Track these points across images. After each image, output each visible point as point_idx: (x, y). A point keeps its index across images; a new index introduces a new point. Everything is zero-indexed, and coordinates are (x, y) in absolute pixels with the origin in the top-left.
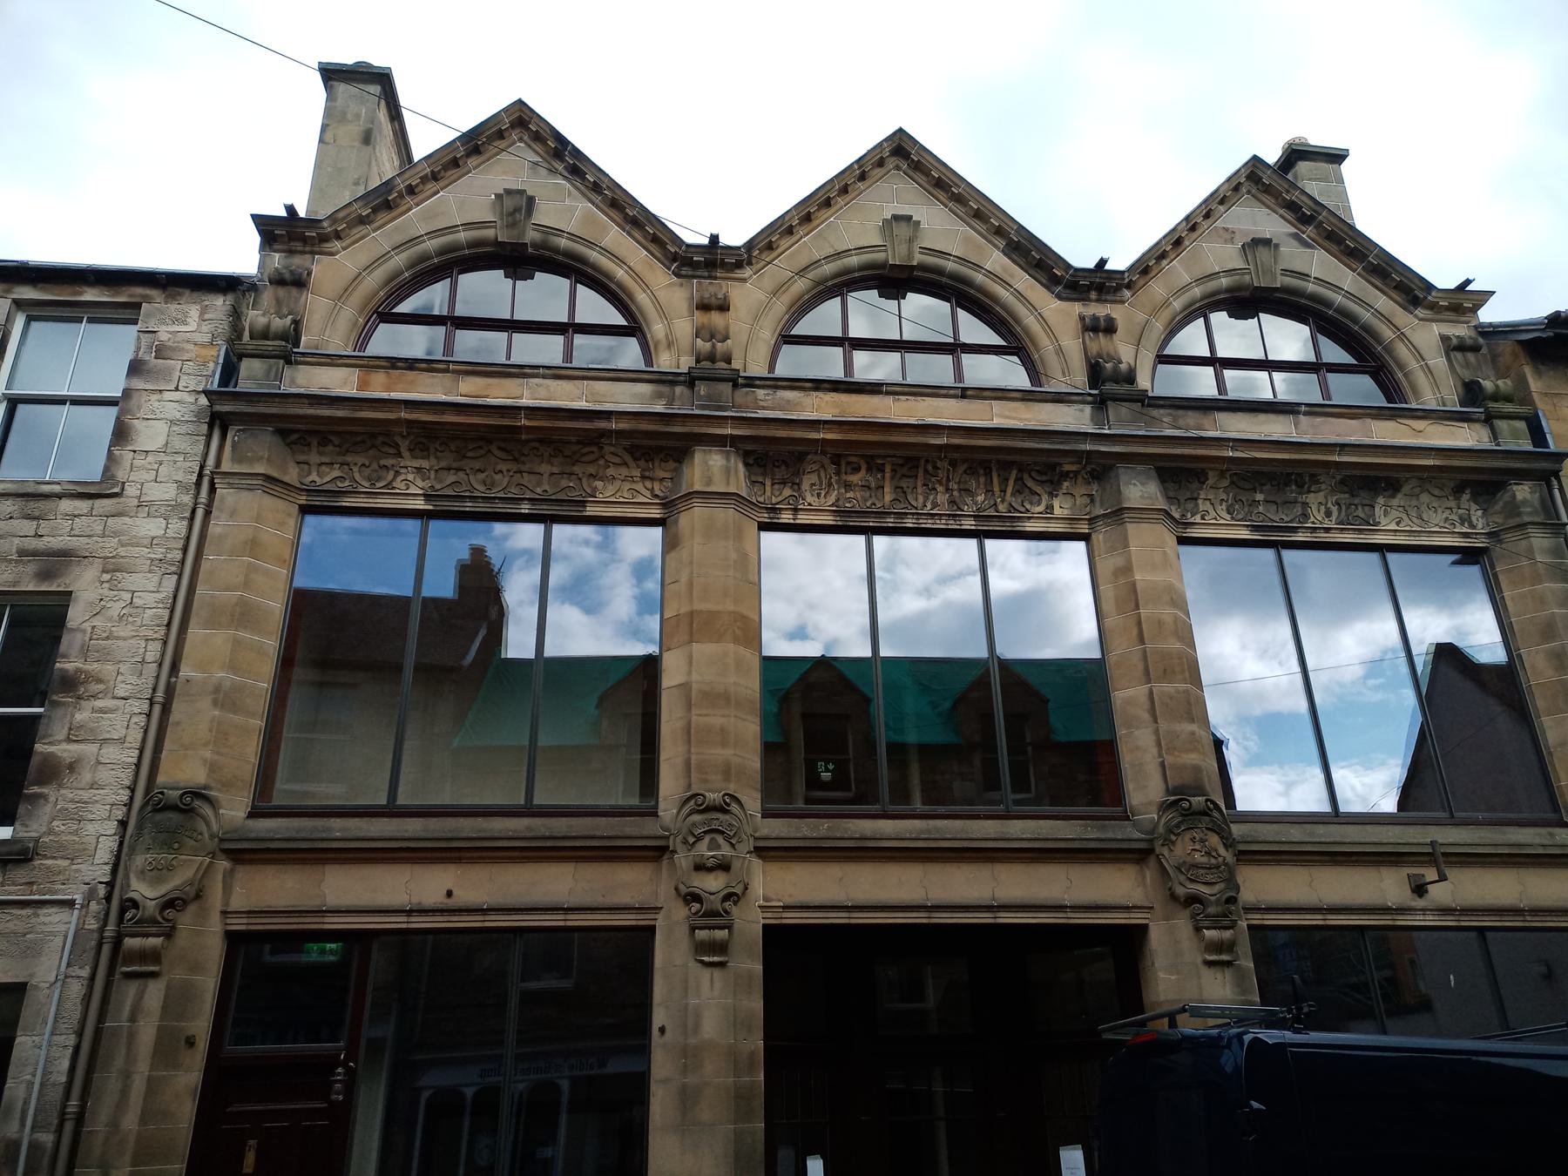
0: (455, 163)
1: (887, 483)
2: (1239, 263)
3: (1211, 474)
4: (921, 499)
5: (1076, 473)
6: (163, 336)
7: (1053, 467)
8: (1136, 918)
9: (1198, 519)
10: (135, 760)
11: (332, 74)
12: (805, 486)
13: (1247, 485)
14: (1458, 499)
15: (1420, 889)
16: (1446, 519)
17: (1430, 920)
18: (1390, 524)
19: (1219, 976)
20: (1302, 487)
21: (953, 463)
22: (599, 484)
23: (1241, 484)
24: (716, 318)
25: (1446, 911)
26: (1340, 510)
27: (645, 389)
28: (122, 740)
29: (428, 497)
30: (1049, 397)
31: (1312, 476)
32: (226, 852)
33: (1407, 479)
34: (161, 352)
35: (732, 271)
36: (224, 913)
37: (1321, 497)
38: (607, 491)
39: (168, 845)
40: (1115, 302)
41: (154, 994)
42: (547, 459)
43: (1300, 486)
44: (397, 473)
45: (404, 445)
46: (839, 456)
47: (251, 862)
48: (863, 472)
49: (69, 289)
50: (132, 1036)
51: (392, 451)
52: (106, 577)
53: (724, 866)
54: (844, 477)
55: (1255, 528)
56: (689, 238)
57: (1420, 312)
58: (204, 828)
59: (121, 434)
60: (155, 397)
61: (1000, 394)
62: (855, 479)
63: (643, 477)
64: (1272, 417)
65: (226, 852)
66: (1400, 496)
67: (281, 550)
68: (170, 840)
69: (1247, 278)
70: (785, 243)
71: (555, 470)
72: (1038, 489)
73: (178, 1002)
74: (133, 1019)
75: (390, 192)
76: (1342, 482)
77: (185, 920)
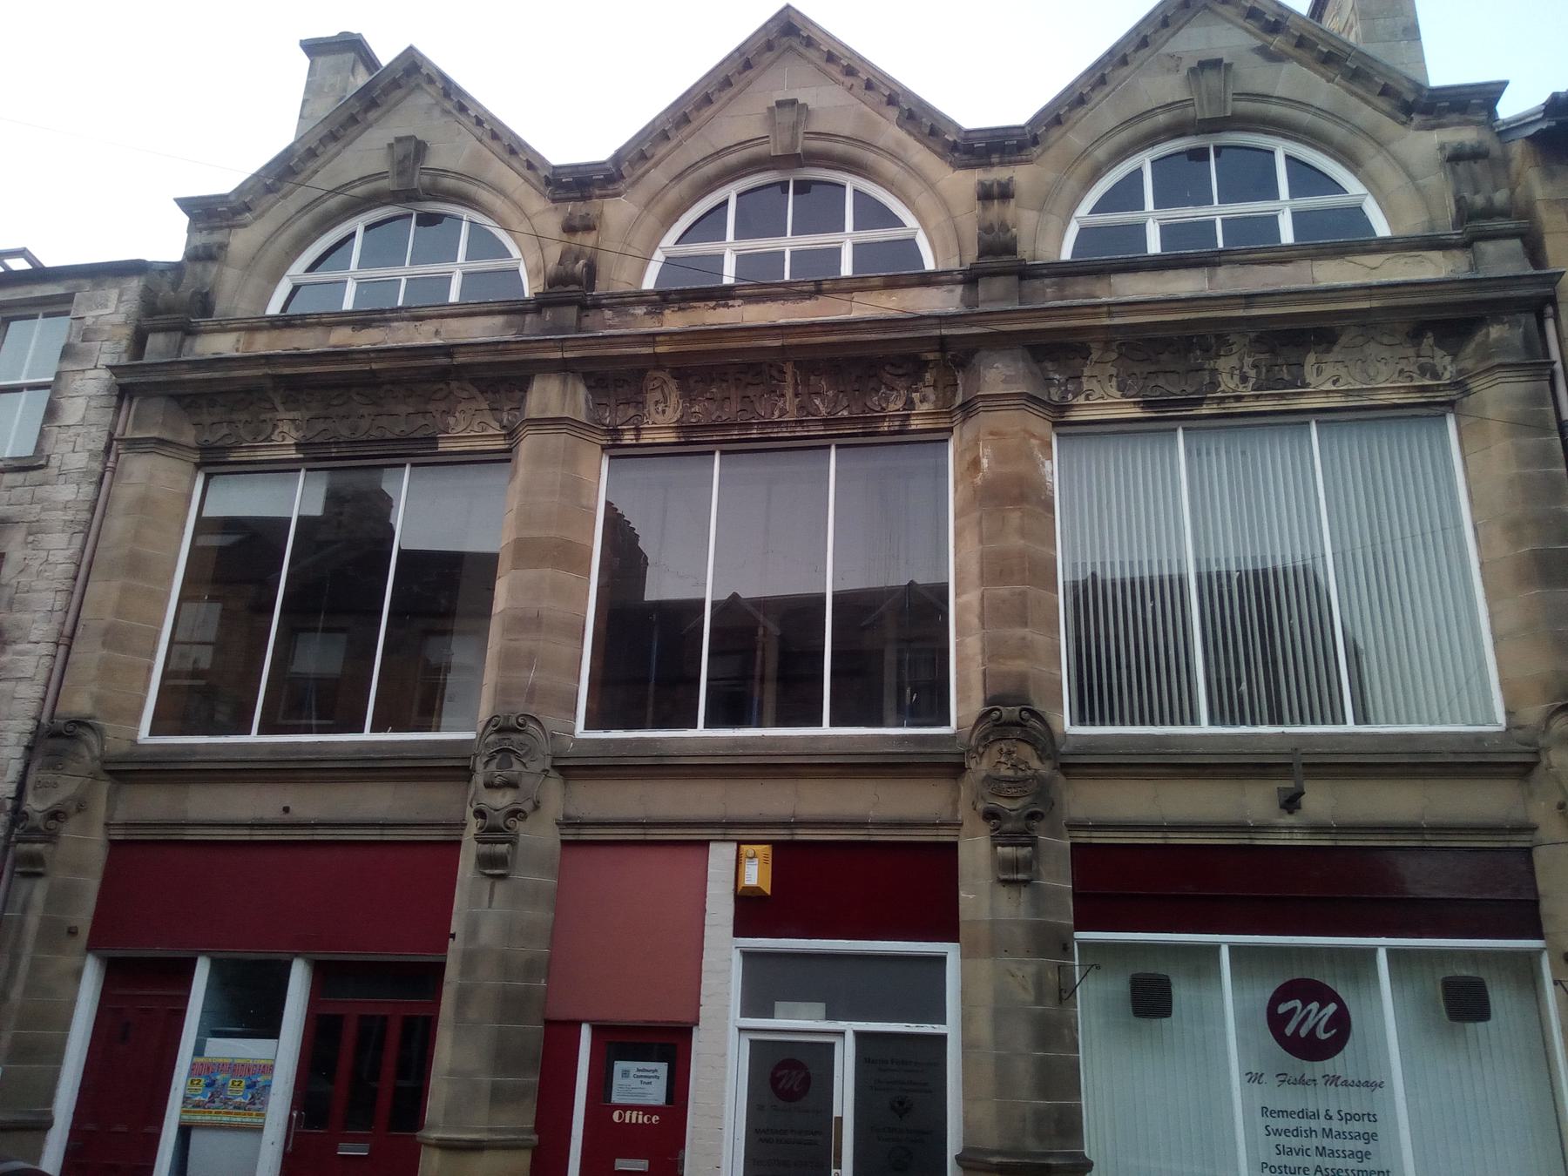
0: (353, 120)
2: (1180, 94)
6: (89, 321)
8: (944, 836)
9: (1081, 400)
10: (40, 695)
11: (314, 48)
16: (1401, 372)
17: (1299, 840)
18: (1326, 379)
22: (451, 420)
24: (588, 240)
25: (1318, 829)
26: (1259, 373)
28: (31, 679)
29: (299, 446)
31: (1218, 337)
32: (110, 772)
34: (87, 335)
36: (107, 825)
37: (1233, 361)
39: (52, 766)
41: (39, 891)
44: (275, 426)
45: (277, 401)
47: (133, 782)
50: (21, 924)
51: (268, 406)
52: (31, 538)
53: (511, 785)
55: (1147, 405)
58: (86, 753)
59: (51, 413)
60: (78, 377)
64: (1183, 272)
65: (110, 772)
66: (1336, 348)
67: (185, 505)
68: (55, 761)
69: (1191, 109)
70: (662, 150)
71: (411, 410)
73: (61, 898)
74: (24, 910)
76: (1259, 340)
77: (69, 831)
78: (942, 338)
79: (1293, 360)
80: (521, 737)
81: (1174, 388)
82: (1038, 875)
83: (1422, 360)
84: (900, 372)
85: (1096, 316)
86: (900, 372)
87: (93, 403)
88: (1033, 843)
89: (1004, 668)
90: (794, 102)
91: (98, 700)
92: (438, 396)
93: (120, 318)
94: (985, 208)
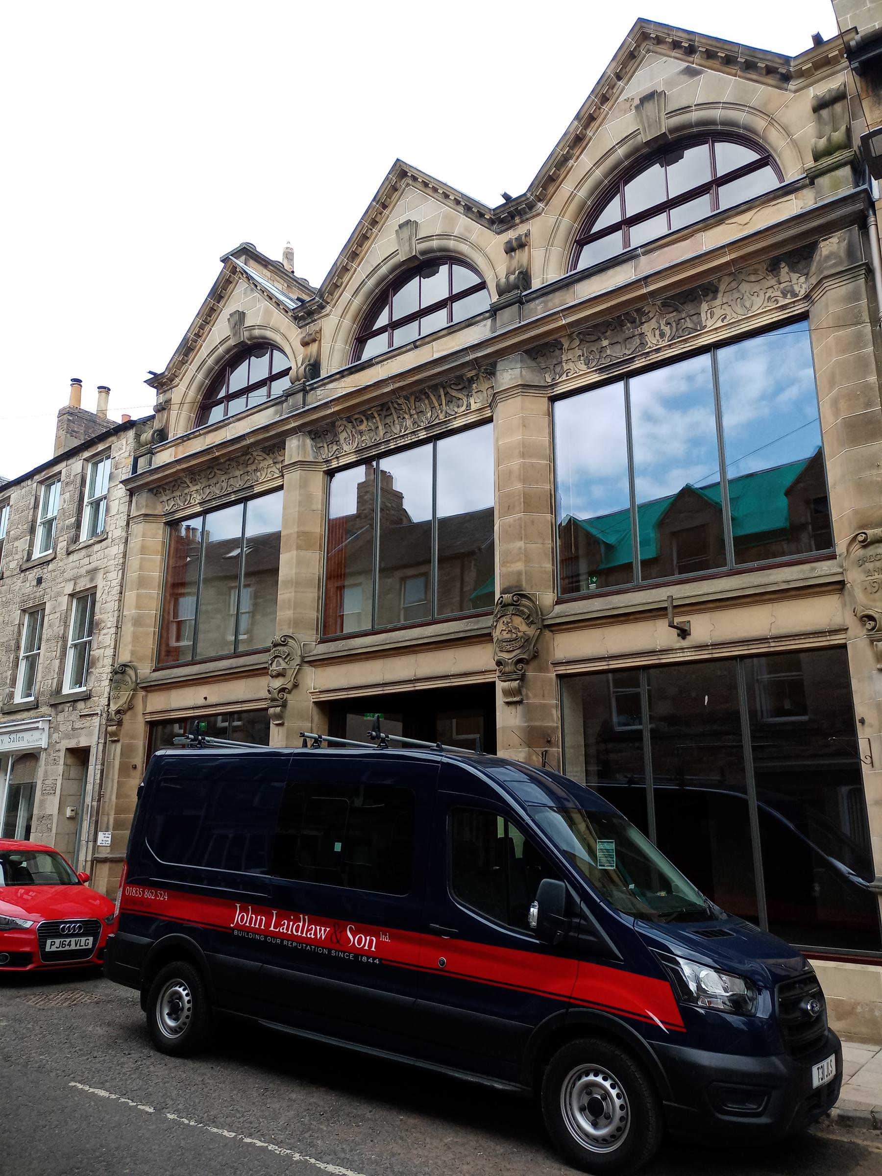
1: (379, 424)
3: (563, 340)
4: (398, 427)
5: (477, 375)
7: (460, 378)
8: (837, 639)
9: (564, 377)
12: (342, 441)
13: (594, 338)
14: (777, 275)
15: (684, 633)
17: (689, 656)
18: (714, 319)
19: (514, 711)
20: (634, 322)
21: (407, 398)
22: (259, 474)
23: (588, 338)
26: (671, 329)
27: (271, 410)
30: (463, 325)
32: (142, 688)
33: (720, 279)
35: (320, 313)
37: (653, 324)
38: (262, 476)
40: (534, 217)
42: (436, 396)
43: (633, 322)
46: (348, 417)
48: (365, 422)
49: (94, 448)
54: (358, 428)
56: (792, 51)
57: (792, 85)
61: (434, 336)
62: (363, 427)
63: (275, 463)
66: (720, 295)
72: (460, 396)
73: (127, 752)
75: (188, 343)
76: (664, 305)
77: (126, 718)
78: (476, 359)
79: (692, 312)
80: (284, 648)
81: (618, 353)
82: (528, 698)
83: (782, 286)
84: (460, 387)
85: (556, 320)
86: (460, 387)
87: (122, 502)
88: (523, 678)
89: (510, 570)
90: (408, 222)
91: (133, 653)
92: (250, 462)
93: (127, 454)
94: (511, 257)
